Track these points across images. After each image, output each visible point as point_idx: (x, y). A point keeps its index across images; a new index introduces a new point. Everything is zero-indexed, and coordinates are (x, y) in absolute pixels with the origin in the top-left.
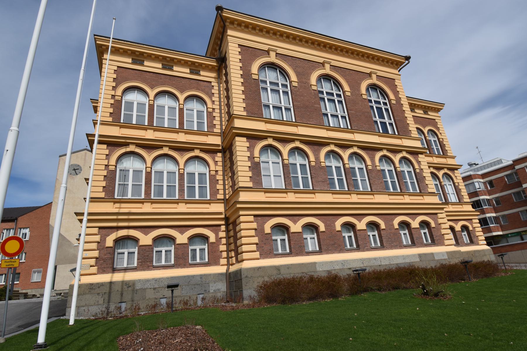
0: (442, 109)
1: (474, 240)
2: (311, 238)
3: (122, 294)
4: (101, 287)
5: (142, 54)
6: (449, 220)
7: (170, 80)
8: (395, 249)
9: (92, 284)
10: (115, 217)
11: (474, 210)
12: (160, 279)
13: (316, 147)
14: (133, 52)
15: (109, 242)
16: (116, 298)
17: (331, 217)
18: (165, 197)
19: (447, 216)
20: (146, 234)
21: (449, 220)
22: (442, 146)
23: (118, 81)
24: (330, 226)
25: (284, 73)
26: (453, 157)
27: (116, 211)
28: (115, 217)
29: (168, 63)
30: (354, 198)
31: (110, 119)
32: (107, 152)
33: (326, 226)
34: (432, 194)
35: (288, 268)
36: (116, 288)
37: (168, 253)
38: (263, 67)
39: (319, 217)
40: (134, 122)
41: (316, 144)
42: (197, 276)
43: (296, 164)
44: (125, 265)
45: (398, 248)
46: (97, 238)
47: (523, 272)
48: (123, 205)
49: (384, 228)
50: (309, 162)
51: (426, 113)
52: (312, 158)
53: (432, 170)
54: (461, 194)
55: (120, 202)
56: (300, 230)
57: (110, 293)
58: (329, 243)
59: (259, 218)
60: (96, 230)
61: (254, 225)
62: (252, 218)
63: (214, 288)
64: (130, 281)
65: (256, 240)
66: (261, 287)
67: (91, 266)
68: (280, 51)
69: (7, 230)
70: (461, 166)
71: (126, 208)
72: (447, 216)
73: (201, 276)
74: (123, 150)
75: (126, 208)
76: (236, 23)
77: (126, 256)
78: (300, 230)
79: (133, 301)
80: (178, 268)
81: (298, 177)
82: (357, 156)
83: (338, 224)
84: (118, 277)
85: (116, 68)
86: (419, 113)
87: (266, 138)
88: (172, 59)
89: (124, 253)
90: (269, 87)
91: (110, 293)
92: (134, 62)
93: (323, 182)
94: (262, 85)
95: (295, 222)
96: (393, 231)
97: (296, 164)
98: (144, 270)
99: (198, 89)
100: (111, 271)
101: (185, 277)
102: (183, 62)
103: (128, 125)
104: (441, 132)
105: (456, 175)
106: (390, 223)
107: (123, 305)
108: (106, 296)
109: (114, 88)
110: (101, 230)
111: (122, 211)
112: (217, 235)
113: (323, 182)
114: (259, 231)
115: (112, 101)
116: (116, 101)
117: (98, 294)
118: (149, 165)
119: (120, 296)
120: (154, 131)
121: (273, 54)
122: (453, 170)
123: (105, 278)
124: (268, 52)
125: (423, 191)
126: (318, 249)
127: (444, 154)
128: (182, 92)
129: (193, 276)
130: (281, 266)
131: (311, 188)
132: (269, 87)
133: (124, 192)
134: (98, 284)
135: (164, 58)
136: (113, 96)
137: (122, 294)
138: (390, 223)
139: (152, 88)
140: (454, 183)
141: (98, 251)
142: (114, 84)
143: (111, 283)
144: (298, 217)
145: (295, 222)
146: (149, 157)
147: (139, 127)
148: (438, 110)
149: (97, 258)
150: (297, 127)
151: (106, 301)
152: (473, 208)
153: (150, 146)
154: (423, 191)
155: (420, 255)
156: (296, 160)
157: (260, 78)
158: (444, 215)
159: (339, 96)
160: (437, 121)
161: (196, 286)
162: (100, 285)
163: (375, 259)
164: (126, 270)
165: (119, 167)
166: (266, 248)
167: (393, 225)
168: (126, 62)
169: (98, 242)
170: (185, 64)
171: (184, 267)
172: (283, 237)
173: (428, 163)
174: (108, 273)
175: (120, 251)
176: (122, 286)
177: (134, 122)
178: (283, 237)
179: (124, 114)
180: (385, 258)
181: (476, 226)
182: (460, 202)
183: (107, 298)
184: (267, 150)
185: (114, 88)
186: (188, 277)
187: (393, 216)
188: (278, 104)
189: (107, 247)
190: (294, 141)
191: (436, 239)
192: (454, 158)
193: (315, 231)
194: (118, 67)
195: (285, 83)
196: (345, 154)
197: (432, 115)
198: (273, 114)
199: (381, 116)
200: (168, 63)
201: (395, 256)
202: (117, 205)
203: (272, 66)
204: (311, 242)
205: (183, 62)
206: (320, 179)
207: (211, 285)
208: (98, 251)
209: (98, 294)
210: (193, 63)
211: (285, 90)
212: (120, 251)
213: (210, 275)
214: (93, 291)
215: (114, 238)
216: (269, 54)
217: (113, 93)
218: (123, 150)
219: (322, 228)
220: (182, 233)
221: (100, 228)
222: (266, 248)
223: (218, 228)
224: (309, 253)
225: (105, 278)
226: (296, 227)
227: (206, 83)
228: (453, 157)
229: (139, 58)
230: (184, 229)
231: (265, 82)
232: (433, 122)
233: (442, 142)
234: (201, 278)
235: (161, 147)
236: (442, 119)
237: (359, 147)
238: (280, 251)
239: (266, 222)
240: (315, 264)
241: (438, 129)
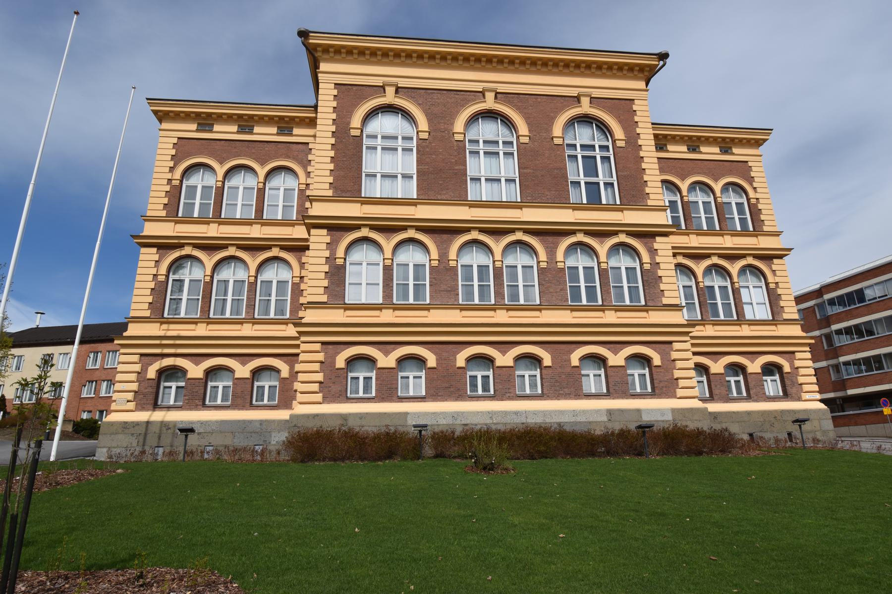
0: (765, 140)
1: (792, 390)
2: (595, 375)
3: (159, 437)
4: (136, 428)
5: (209, 115)
6: (695, 354)
7: (248, 147)
8: (566, 399)
9: (126, 423)
10: (158, 342)
11: (804, 334)
12: (207, 422)
13: (550, 239)
14: (198, 114)
15: (152, 373)
16: (152, 441)
17: (451, 346)
18: (228, 315)
19: (693, 345)
20: (197, 364)
21: (695, 354)
22: (755, 212)
23: (176, 159)
24: (561, 360)
25: (507, 122)
26: (777, 234)
27: (162, 333)
28: (158, 342)
29: (246, 123)
30: (610, 317)
31: (164, 213)
32: (156, 257)
33: (438, 361)
34: (676, 307)
35: (361, 418)
36: (152, 429)
37: (167, 390)
38: (571, 123)
39: (430, 346)
40: (196, 215)
41: (550, 233)
42: (256, 421)
43: (620, 268)
44: (172, 402)
45: (571, 398)
46: (137, 368)
47: (890, 457)
48: (172, 326)
49: (550, 364)
50: (641, 264)
51: (726, 150)
52: (543, 256)
53: (681, 260)
54: (778, 305)
55: (169, 322)
56: (623, 363)
57: (146, 434)
58: (446, 384)
59: (330, 347)
60: (136, 358)
61: (321, 357)
62: (318, 347)
63: (277, 439)
64: (170, 422)
65: (320, 377)
66: (664, 433)
67: (128, 401)
68: (596, 93)
69: (94, 352)
70: (790, 250)
71: (175, 330)
72: (693, 345)
73: (261, 422)
74: (176, 254)
75: (175, 330)
76: (551, 63)
77: (171, 390)
78: (511, 364)
79: (172, 446)
80: (234, 409)
81: (622, 287)
82: (625, 248)
83: (575, 358)
84: (158, 416)
85: (175, 141)
86: (677, 151)
87: (616, 233)
88: (251, 117)
89: (171, 387)
90: (579, 153)
91: (146, 434)
92: (202, 127)
93: (447, 291)
94: (569, 152)
95: (386, 354)
96: (569, 370)
97: (620, 268)
98: (191, 409)
99: (287, 157)
100: (151, 407)
101: (239, 421)
102: (307, 120)
103: (189, 220)
104: (755, 185)
105: (774, 267)
106: (565, 357)
107: (161, 450)
108: (141, 439)
109: (172, 169)
110: (143, 358)
111: (170, 334)
112: (292, 368)
113: (447, 291)
114: (327, 365)
115: (168, 188)
116: (173, 187)
117: (132, 434)
118: (253, 273)
119: (157, 440)
120: (219, 224)
121: (585, 101)
122: (768, 258)
123: (142, 416)
124: (577, 99)
125: (653, 302)
126: (605, 391)
127: (758, 230)
128: (262, 163)
129: (250, 422)
130: (350, 414)
131: (643, 303)
132: (579, 153)
133: (177, 311)
134: (133, 422)
135: (240, 116)
136: (170, 181)
137: (159, 437)
138: (565, 357)
139: (221, 163)
140: (767, 284)
141: (137, 384)
142: (171, 164)
143: (148, 423)
144: (393, 346)
145: (386, 354)
146: (253, 262)
147: (202, 221)
148: (758, 143)
149: (136, 392)
150: (622, 211)
151: (141, 443)
152: (803, 330)
153: (253, 247)
154: (653, 302)
155: (610, 412)
156: (620, 262)
157: (567, 142)
158: (687, 346)
159: (604, 148)
160: (750, 164)
161: (253, 435)
162: (136, 424)
163: (516, 413)
164: (169, 408)
165: (172, 277)
166: (336, 388)
167: (569, 360)
168: (189, 129)
169: (139, 373)
170: (228, 119)
171: (242, 409)
172: (642, 372)
173: (673, 248)
174: (148, 410)
175: (167, 384)
176: (161, 427)
177: (196, 215)
178: (642, 372)
179: (185, 203)
180: (535, 413)
181: (805, 366)
182: (776, 319)
183: (141, 440)
184: (618, 250)
185: (172, 169)
186: (244, 422)
187: (573, 346)
188: (494, 175)
189: (149, 379)
190: (575, 233)
191: (663, 386)
192: (778, 235)
193: (602, 366)
194: (179, 138)
195: (605, 143)
196: (602, 248)
197: (739, 153)
198: (485, 192)
199: (590, 168)
200: (246, 123)
201: (556, 411)
202: (165, 326)
203: (586, 119)
204: (593, 379)
205: (266, 119)
206: (443, 287)
207: (273, 434)
208: (137, 384)
209: (132, 434)
210: (281, 118)
211: (605, 154)
212: (167, 384)
213: (274, 421)
214: (126, 431)
215: (158, 368)
216: (579, 101)
217: (169, 176)
218: (176, 254)
219: (547, 361)
220: (244, 364)
221: (142, 355)
222: (336, 388)
223: (295, 358)
224: (589, 396)
225: (142, 416)
226: (616, 359)
227: (300, 146)
228: (777, 234)
229: (205, 121)
230: (247, 358)
231: (575, 146)
232: (743, 168)
233: (755, 205)
234: (261, 424)
235: (225, 247)
236: (761, 162)
237: (630, 234)
238: (638, 390)
239: (339, 353)
240: (406, 414)
241: (751, 180)
